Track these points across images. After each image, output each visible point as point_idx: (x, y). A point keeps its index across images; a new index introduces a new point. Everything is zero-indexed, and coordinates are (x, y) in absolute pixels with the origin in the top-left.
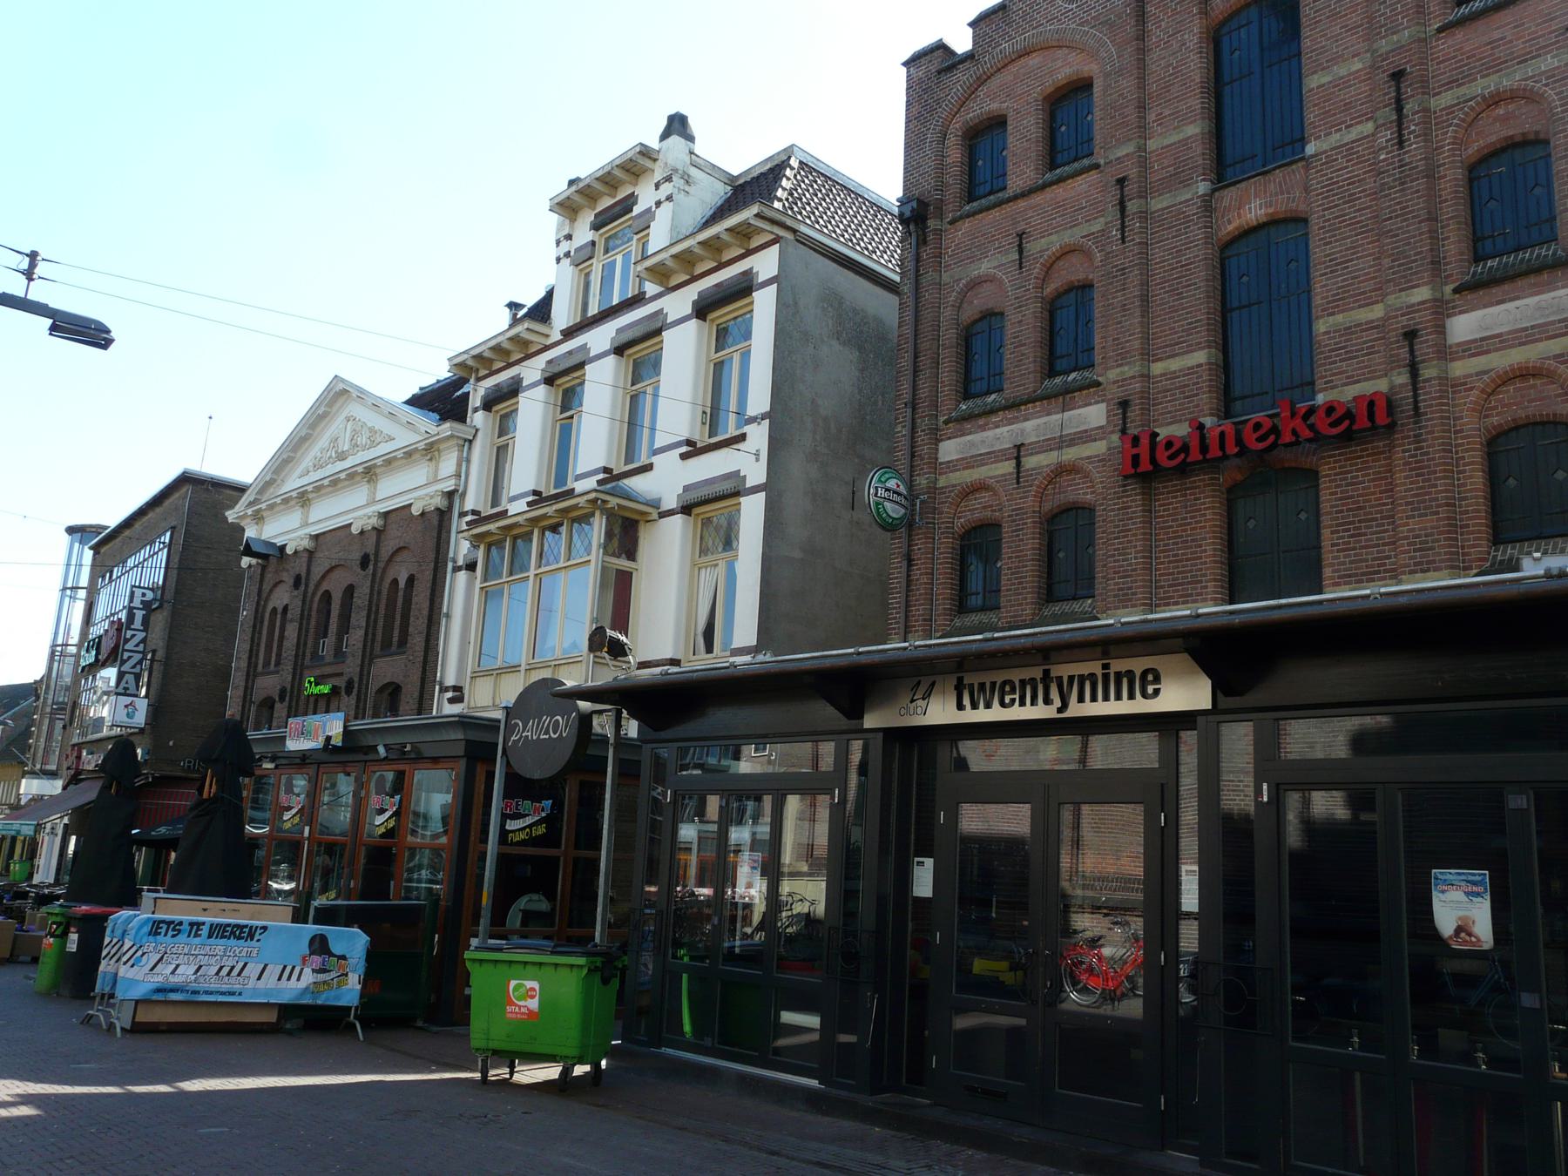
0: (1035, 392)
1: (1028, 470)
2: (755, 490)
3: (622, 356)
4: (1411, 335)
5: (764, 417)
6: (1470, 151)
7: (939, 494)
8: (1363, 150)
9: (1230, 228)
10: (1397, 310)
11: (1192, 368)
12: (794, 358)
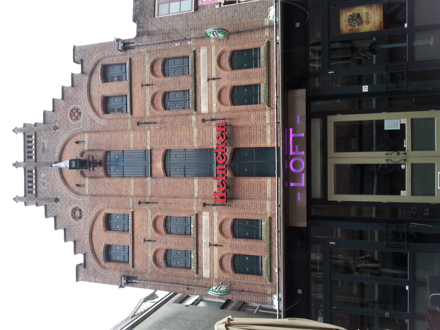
1: (218, 242)
8: (153, 133)
9: (162, 172)
10: (196, 124)
11: (198, 183)
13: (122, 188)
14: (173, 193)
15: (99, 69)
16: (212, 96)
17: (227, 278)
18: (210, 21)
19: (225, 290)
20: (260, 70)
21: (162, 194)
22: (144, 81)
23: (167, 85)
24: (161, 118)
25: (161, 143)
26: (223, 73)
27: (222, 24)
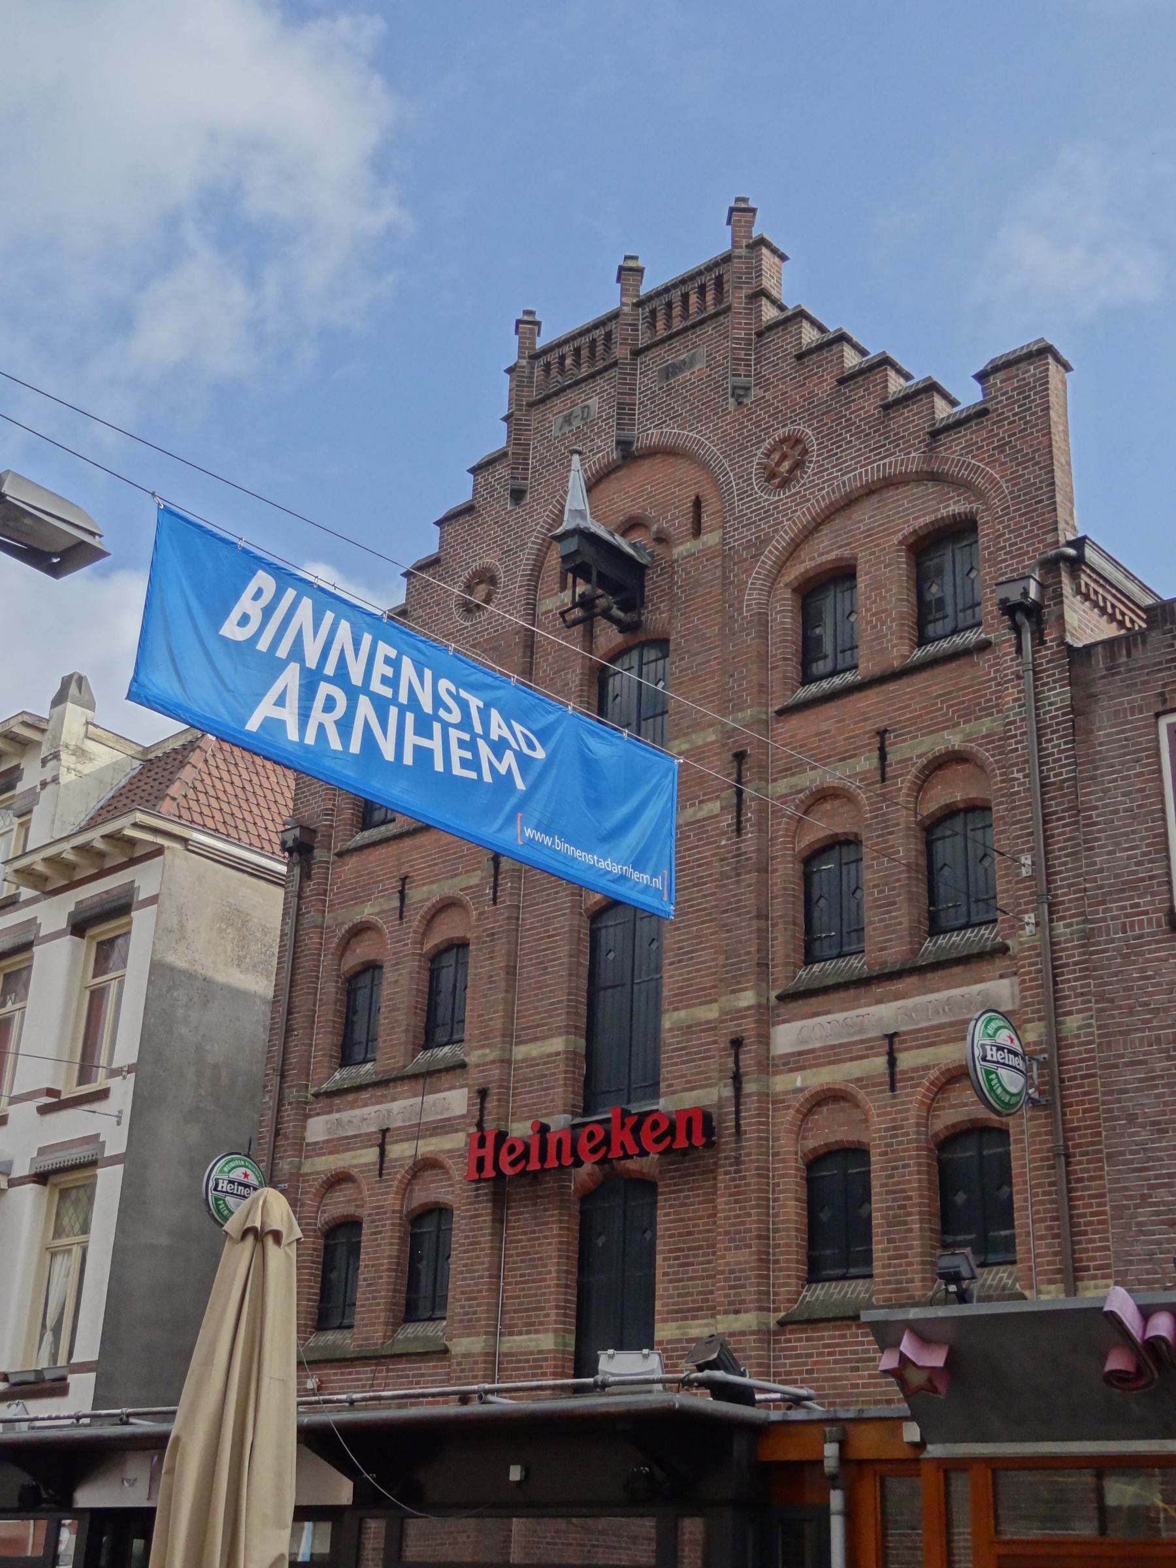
0: (405, 1067)
2: (114, 1160)
3: (82, 937)
4: (737, 1044)
5: (131, 1069)
6: (803, 845)
7: (304, 1181)
12: (175, 994)
15: (955, 507)
16: (831, 1063)
18: (1120, 1007)
19: (1005, 1090)
20: (915, 1272)
24: (754, 851)
26: (911, 1102)
27: (1103, 1067)
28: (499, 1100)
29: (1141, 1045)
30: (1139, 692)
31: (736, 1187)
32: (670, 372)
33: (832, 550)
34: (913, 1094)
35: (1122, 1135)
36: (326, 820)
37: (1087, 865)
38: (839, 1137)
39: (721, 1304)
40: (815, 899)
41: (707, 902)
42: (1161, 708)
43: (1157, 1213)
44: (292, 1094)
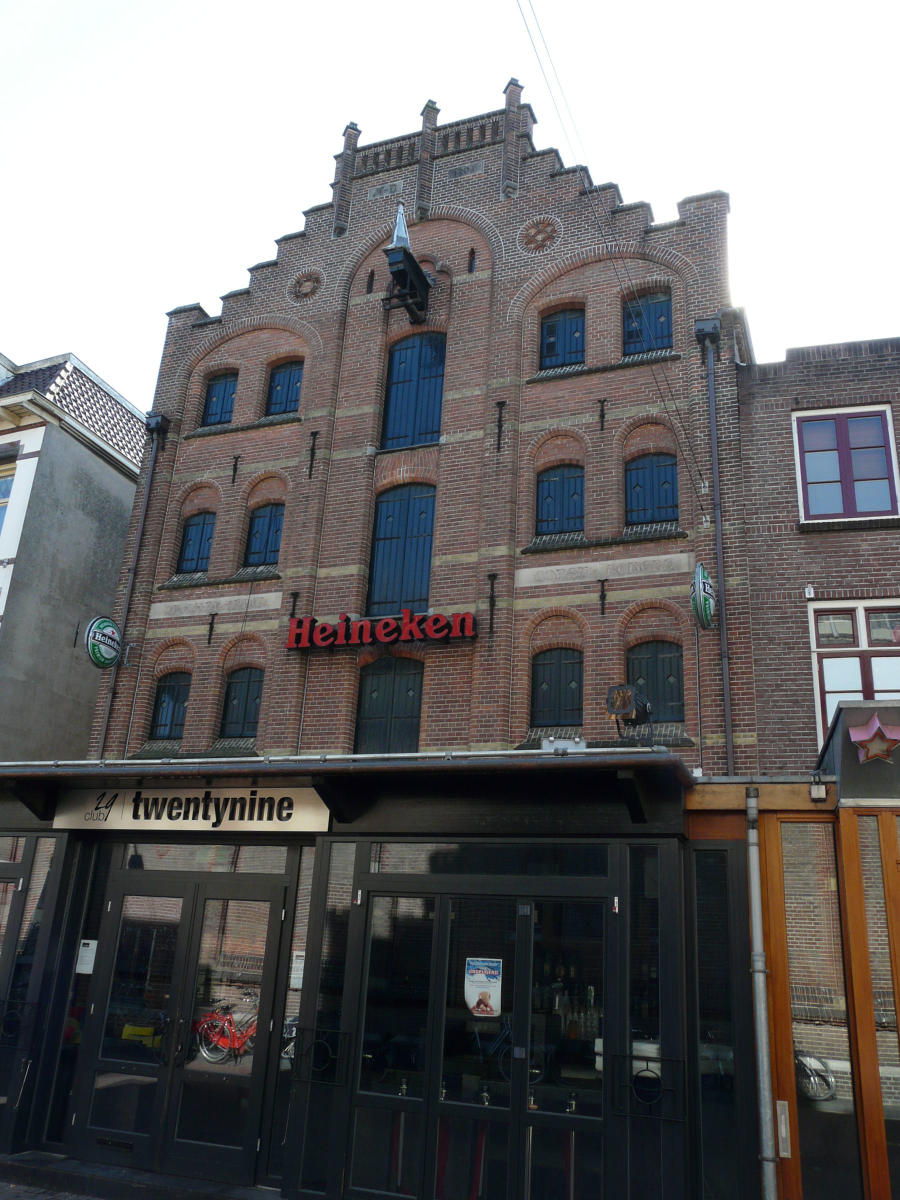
1: (218, 634)
4: (493, 577)
9: (385, 482)
10: (485, 558)
12: (43, 519)
13: (355, 385)
14: (332, 516)
15: (657, 276)
17: (146, 659)
18: (765, 575)
21: (332, 486)
22: (614, 404)
23: (597, 470)
25: (451, 470)
27: (753, 609)
28: (308, 601)
29: (779, 598)
30: (782, 395)
31: (488, 665)
32: (455, 173)
33: (570, 291)
34: (617, 617)
35: (765, 649)
36: (178, 415)
37: (746, 491)
38: (560, 640)
39: (473, 736)
40: (255, 532)
41: (470, 491)
42: (795, 407)
43: (786, 696)
44: (141, 587)
